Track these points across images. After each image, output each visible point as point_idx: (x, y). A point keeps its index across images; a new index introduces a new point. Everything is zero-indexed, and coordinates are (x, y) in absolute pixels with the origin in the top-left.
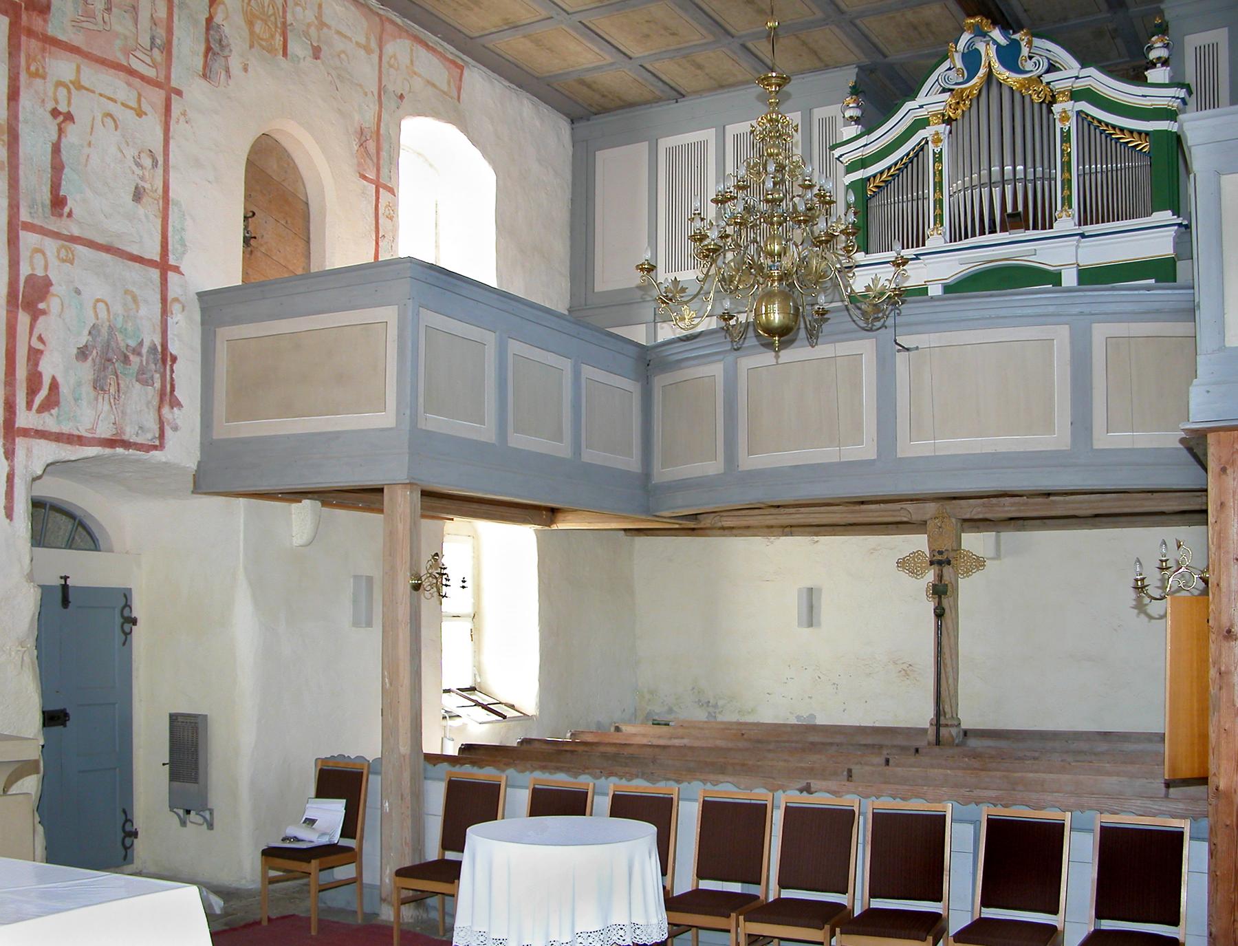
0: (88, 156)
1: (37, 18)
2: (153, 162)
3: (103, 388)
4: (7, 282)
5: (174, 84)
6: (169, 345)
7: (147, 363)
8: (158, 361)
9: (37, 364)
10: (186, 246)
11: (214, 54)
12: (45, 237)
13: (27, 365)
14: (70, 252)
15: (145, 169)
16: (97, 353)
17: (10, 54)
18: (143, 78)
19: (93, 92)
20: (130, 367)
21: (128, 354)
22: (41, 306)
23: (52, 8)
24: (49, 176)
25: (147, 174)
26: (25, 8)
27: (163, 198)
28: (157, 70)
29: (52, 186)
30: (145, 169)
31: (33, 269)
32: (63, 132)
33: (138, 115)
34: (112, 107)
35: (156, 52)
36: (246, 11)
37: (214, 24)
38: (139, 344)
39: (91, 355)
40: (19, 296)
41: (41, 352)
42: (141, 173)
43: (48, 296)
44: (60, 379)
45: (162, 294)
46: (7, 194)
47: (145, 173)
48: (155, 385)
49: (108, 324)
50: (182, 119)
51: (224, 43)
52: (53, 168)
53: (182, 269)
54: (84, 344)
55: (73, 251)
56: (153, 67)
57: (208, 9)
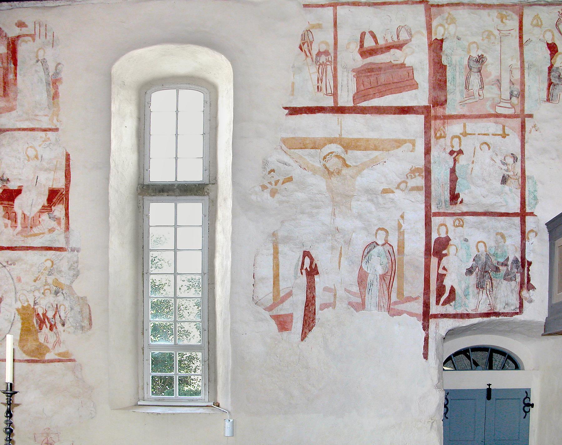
7: (511, 269)
8: (519, 266)
9: (443, 281)
16: (479, 269)
18: (505, 116)
22: (444, 252)
25: (510, 167)
31: (439, 235)
33: (503, 137)
34: (486, 139)
35: (514, 100)
41: (445, 275)
45: (521, 230)
49: (485, 253)
50: (533, 129)
52: (451, 181)
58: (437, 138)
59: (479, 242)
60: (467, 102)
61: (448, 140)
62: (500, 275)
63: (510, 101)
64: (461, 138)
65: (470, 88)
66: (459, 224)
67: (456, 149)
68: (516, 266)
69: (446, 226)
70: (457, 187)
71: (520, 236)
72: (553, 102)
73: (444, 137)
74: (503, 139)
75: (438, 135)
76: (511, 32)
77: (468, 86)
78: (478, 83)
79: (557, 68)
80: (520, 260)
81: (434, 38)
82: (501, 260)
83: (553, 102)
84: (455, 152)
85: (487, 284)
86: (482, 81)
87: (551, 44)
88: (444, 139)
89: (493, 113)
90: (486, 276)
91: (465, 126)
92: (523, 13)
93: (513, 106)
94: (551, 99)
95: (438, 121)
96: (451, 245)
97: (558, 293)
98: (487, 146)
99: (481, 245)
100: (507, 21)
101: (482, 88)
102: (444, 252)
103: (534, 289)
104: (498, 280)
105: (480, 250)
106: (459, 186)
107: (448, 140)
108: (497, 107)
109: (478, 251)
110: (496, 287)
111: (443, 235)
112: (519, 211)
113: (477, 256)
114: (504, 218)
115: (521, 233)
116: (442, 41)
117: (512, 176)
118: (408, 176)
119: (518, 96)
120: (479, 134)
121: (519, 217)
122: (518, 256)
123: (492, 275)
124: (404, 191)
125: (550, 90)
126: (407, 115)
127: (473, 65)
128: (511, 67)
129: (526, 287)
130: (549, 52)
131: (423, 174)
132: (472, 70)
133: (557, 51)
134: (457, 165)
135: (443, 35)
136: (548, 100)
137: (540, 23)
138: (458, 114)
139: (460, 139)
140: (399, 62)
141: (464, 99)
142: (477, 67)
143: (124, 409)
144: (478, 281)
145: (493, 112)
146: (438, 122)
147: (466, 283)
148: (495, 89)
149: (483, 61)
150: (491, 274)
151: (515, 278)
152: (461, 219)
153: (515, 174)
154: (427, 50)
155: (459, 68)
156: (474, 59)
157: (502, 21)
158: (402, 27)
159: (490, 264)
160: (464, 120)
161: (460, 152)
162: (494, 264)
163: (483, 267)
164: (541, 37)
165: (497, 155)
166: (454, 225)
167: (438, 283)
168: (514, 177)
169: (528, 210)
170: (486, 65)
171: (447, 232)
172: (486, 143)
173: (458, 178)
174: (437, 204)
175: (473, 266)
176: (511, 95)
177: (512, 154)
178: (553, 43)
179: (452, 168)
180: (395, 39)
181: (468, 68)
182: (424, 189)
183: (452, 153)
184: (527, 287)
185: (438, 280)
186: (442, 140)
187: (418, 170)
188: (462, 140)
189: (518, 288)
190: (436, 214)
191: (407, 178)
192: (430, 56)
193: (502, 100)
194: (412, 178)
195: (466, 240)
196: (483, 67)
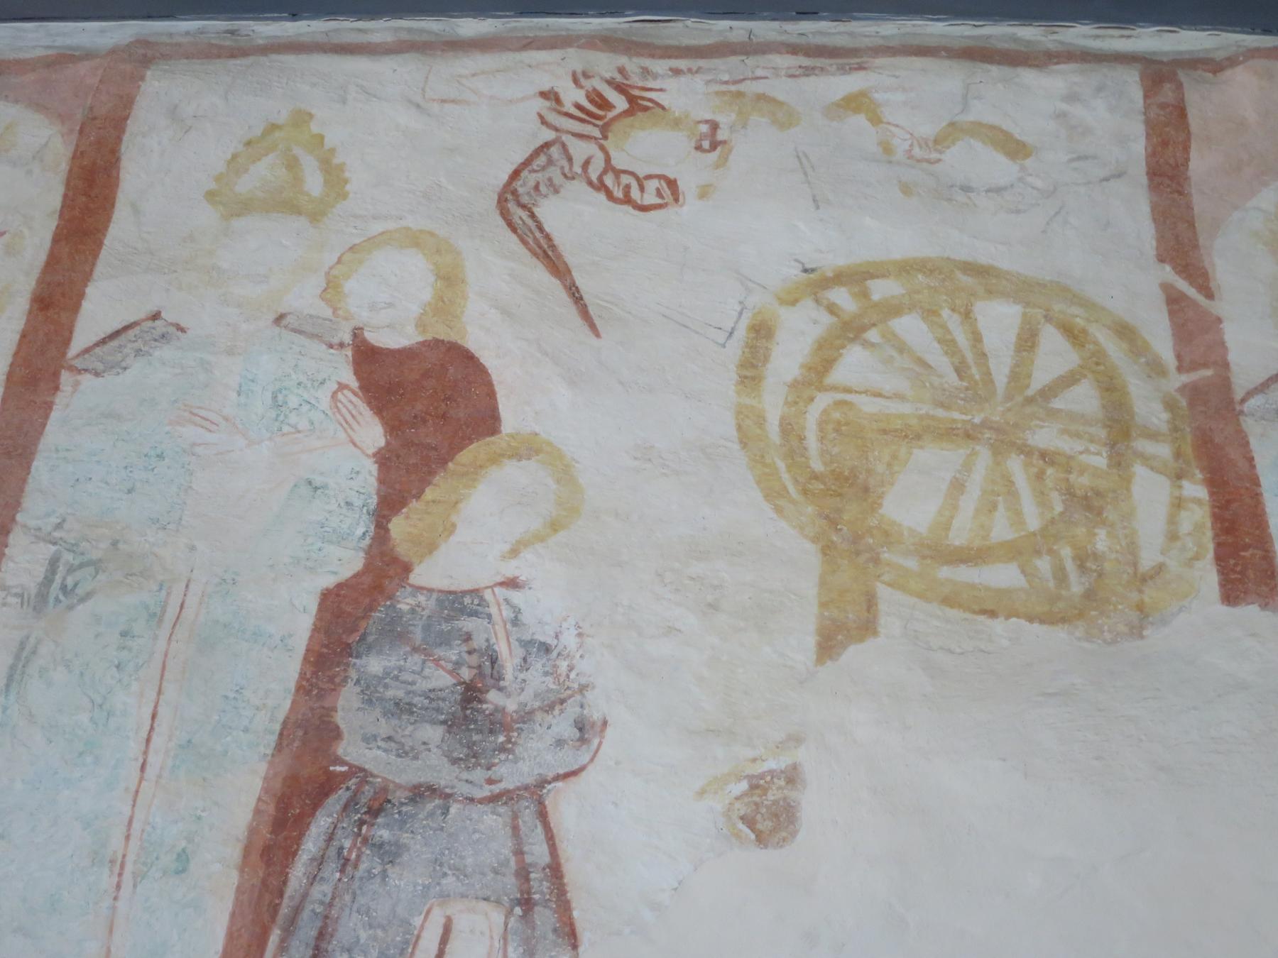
26: (433, 656)
36: (787, 428)
92: (127, 103)
125: (298, 872)
130: (373, 434)
133: (488, 422)
143: (717, 343)
178: (437, 343)
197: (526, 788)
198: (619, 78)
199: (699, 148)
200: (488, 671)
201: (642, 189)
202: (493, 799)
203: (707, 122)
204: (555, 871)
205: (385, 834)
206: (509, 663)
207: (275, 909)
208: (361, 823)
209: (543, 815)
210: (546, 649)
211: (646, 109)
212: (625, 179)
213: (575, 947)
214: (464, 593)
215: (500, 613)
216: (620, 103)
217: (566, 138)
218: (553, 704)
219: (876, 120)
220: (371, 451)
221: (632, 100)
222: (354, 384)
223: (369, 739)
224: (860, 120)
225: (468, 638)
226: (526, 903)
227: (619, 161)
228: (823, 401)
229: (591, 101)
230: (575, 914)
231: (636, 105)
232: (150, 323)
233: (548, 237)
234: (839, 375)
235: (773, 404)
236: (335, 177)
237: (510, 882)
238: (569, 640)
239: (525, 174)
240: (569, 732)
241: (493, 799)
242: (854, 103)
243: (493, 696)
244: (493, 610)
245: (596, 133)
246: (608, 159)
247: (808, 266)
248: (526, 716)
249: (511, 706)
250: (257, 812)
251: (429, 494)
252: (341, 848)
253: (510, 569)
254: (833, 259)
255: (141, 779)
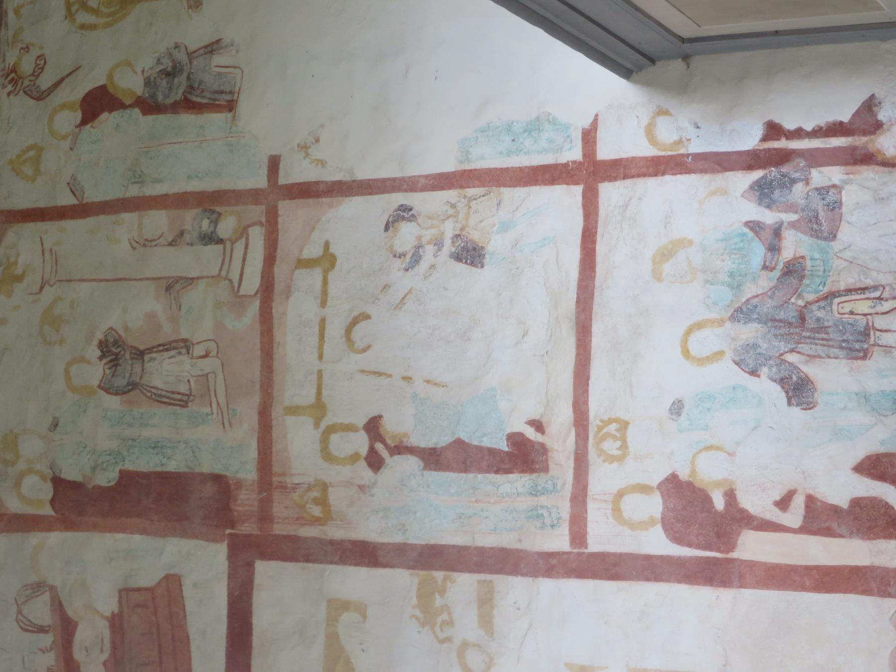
0: (428, 382)
1: (239, 502)
2: (403, 218)
3: (860, 333)
4: (687, 586)
5: (260, 181)
6: (746, 148)
7: (791, 208)
8: (784, 176)
9: (835, 510)
10: (538, 119)
11: (191, 88)
12: (590, 493)
13: (841, 536)
14: (605, 430)
15: (419, 238)
16: (792, 351)
17: (307, 559)
18: (270, 260)
19: (320, 374)
20: (808, 258)
21: (781, 266)
22: (719, 503)
23: (216, 471)
24: (480, 476)
25: (428, 234)
26: (232, 527)
27: (462, 187)
28: (249, 226)
29: (497, 472)
30: (419, 238)
31: (652, 522)
32: (401, 442)
33: (333, 266)
34: (335, 331)
35: (227, 227)
36: (109, 15)
37: (147, 95)
38: (756, 233)
39: (796, 368)
40: (707, 558)
41: (811, 500)
42: (429, 249)
43: (698, 484)
44: (859, 453)
45: (644, 175)
46: (530, 579)
47: (428, 238)
48: (837, 182)
49: (728, 324)
50: (315, 152)
51: (168, 64)
52: (465, 468)
53: (587, 123)
54: (779, 388)
55: (602, 421)
56: (248, 235)
57: (128, 111)
58: (326, 517)
59: (686, 353)
60: (222, 400)
61: (336, 474)
62: (817, 256)
63: (228, 244)
64: (331, 423)
65: (183, 389)
66: (615, 438)
67: (360, 442)
68: (782, 186)
69: (620, 495)
70: (487, 442)
71: (668, 178)
72: (237, 89)
73: (324, 487)
74: (338, 264)
75: (316, 511)
76: (47, 246)
77: (179, 397)
78: (172, 360)
79: (148, 83)
80: (757, 174)
81: (48, 511)
82: (758, 252)
83: (237, 89)
84: (372, 451)
85: (852, 313)
86: (166, 347)
87: (84, 114)
88: (330, 489)
89: (257, 303)
90: (818, 320)
91: (294, 410)
93: (243, 232)
94: (228, 97)
95: (275, 510)
96: (693, 472)
97: (884, 10)
98: (358, 326)
99: (696, 345)
100: (21, 260)
101: (185, 345)
102: (719, 503)
103: (876, 102)
104: (838, 264)
105: (716, 349)
106: (484, 435)
107: (336, 474)
108: (242, 292)
109: (720, 354)
110: (865, 270)
111: (655, 505)
112: (578, 190)
113: (737, 359)
114: (601, 248)
115: (655, 174)
116: (58, 482)
117: (459, 226)
118: (442, 636)
119: (214, 217)
120: (321, 357)
121: (600, 185)
122: (744, 180)
123: (816, 292)
124: (491, 659)
126: (255, 621)
127: (124, 377)
128: (134, 244)
129: (865, 139)
131: (439, 575)
132: (138, 380)
133: (103, 88)
134: (415, 440)
135: (43, 478)
136: (231, 106)
137: (32, 153)
138: (256, 435)
139: (332, 429)
140: (107, 634)
141: (215, 411)
142: (130, 362)
144: (837, 352)
145: (255, 307)
146: (279, 509)
147: (845, 408)
148: (193, 297)
149: (116, 343)
150: (811, 297)
151: (827, 189)
152: (600, 429)
153: (451, 211)
154: (80, 536)
155: (130, 425)
156: (108, 371)
157: (19, 278)
158: (19, 612)
159: (770, 303)
160: (277, 412)
161: (373, 427)
162: (772, 284)
163: (783, 331)
164: (66, 144)
165: (386, 287)
166: (620, 459)
167: (844, 530)
168: (461, 216)
169: (574, 153)
170: (127, 329)
171: (644, 489)
172: (349, 330)
173: (456, 436)
174: (542, 528)
175: (777, 377)
176: (210, 239)
177: (387, 228)
178: (81, 106)
179: (422, 459)
180: (47, 640)
181: (131, 394)
182: (489, 577)
183: (375, 462)
184: (865, 133)
185: (828, 532)
186: (335, 497)
187: (425, 597)
188: (339, 420)
189: (868, 174)
190: (578, 535)
191: (448, 640)
192: (95, 528)
193: (223, 274)
194: (450, 623)
195: (677, 408)
196: (131, 341)
197: (188, 57)
198: (4, 77)
199: (28, 52)
200: (163, 72)
201: (39, 65)
202: (190, 63)
203: (20, 51)
204: (206, 47)
205: (197, 84)
206: (161, 67)
207: (212, 104)
208: (194, 90)
209: (194, 52)
210: (159, 60)
211: (15, 68)
212: (36, 69)
213: (221, 39)
214: (145, 82)
215: (150, 72)
216: (13, 75)
217: (23, 87)
218: (171, 54)
219: (23, 6)
220: (109, 114)
221: (12, 72)
222: (91, 124)
223: (177, 93)
224: (22, 11)
225: (155, 78)
226: (211, 52)
227: (30, 72)
228: (102, 9)
229: (12, 82)
230: (214, 40)
231: (14, 70)
232: (71, 185)
233: (52, 86)
234: (95, 6)
235: (102, 20)
236: (29, 148)
237: (208, 56)
238: (157, 55)
239: (33, 96)
240: (177, 50)
241: (190, 63)
242: (17, 12)
243: (168, 70)
244: (149, 74)
245: (22, 80)
246: (30, 76)
247: (65, 17)
248: (173, 61)
249: (171, 64)
250: (191, 114)
251: (120, 97)
252: (200, 93)
253: (139, 72)
254: (63, 12)
255: (184, 142)
